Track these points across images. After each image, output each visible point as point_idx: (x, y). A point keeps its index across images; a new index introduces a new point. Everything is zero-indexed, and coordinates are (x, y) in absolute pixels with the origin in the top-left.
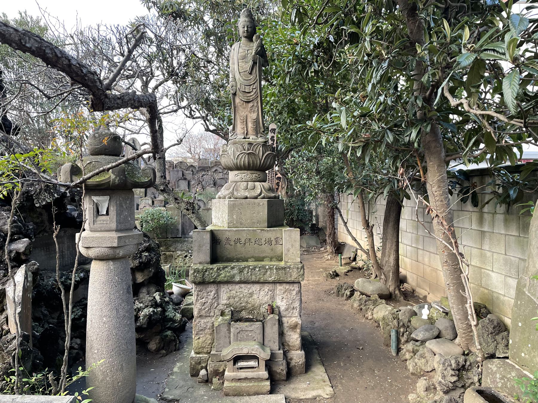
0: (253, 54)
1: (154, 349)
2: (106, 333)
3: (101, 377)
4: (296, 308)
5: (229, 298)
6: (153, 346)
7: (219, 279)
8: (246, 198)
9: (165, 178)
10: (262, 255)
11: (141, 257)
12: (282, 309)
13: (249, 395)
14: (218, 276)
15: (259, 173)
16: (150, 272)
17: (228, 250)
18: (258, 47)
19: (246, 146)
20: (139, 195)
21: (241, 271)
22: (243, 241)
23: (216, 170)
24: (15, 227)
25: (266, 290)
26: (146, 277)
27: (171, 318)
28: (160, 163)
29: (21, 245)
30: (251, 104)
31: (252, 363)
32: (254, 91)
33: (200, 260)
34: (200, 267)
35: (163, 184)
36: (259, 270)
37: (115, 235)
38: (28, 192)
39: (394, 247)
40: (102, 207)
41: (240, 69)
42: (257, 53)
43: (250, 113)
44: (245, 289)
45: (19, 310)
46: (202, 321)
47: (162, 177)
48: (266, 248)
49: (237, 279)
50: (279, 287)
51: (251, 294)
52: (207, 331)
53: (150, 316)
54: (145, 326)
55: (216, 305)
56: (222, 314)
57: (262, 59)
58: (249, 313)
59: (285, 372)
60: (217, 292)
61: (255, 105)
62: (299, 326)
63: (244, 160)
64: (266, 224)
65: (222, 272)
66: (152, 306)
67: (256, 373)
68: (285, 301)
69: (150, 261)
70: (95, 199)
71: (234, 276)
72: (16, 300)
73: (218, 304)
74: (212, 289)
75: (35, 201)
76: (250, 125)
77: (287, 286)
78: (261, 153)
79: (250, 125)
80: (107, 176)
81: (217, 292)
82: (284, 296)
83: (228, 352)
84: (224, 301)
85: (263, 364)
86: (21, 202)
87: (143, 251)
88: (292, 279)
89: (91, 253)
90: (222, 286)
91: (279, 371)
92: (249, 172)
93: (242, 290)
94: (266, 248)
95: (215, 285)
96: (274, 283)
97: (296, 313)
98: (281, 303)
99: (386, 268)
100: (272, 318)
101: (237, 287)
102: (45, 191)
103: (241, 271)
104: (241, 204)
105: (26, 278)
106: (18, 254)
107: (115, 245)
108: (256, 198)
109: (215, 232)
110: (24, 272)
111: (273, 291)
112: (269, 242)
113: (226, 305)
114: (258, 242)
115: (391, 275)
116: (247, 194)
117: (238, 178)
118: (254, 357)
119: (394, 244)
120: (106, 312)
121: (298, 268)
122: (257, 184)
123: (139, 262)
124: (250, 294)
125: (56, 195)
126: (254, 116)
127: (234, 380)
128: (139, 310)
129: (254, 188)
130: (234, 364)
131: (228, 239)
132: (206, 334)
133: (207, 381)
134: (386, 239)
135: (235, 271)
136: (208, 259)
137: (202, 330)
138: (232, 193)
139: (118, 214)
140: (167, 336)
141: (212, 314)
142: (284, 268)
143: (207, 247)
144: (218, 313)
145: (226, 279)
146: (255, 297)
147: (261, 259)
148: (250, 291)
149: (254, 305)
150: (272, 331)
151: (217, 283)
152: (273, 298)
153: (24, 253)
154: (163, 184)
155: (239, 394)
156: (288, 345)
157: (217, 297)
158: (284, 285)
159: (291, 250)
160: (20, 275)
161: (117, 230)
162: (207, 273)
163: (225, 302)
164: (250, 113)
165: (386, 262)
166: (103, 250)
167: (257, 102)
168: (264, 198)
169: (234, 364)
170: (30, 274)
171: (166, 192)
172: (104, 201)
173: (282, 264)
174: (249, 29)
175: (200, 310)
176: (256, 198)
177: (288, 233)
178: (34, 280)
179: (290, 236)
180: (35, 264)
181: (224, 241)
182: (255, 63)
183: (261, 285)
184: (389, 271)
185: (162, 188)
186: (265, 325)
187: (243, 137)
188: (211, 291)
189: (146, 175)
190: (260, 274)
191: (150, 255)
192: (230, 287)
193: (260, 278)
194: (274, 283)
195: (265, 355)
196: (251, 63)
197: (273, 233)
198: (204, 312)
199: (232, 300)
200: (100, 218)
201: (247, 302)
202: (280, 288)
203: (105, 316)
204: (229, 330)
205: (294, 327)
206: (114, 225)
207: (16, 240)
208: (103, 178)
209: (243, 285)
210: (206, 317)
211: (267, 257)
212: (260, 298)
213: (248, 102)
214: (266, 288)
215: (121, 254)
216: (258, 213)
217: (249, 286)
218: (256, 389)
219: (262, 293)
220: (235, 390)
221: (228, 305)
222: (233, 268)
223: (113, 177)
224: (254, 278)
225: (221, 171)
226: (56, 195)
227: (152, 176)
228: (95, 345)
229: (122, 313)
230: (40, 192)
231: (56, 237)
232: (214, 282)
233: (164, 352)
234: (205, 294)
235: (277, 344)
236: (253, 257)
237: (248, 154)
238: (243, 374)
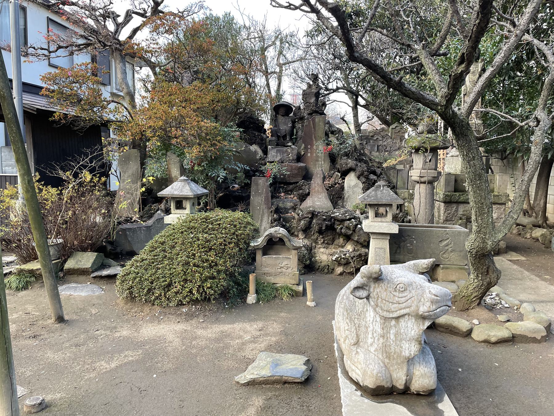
0: (479, 70)
4: (503, 218)
5: (464, 211)
7: (460, 200)
23: (377, 138)
33: (448, 190)
34: (449, 194)
39: (544, 194)
60: (457, 208)
65: (461, 197)
74: (454, 207)
81: (457, 208)
82: (496, 211)
88: (502, 202)
90: (460, 204)
99: (536, 209)
113: (462, 214)
115: (541, 214)
119: (545, 192)
134: (539, 189)
136: (453, 190)
141: (453, 219)
145: (463, 201)
157: (457, 211)
163: (461, 213)
165: (538, 204)
177: (501, 176)
179: (502, 178)
184: (540, 211)
188: (454, 207)
198: (449, 218)
199: (465, 213)
225: (381, 139)
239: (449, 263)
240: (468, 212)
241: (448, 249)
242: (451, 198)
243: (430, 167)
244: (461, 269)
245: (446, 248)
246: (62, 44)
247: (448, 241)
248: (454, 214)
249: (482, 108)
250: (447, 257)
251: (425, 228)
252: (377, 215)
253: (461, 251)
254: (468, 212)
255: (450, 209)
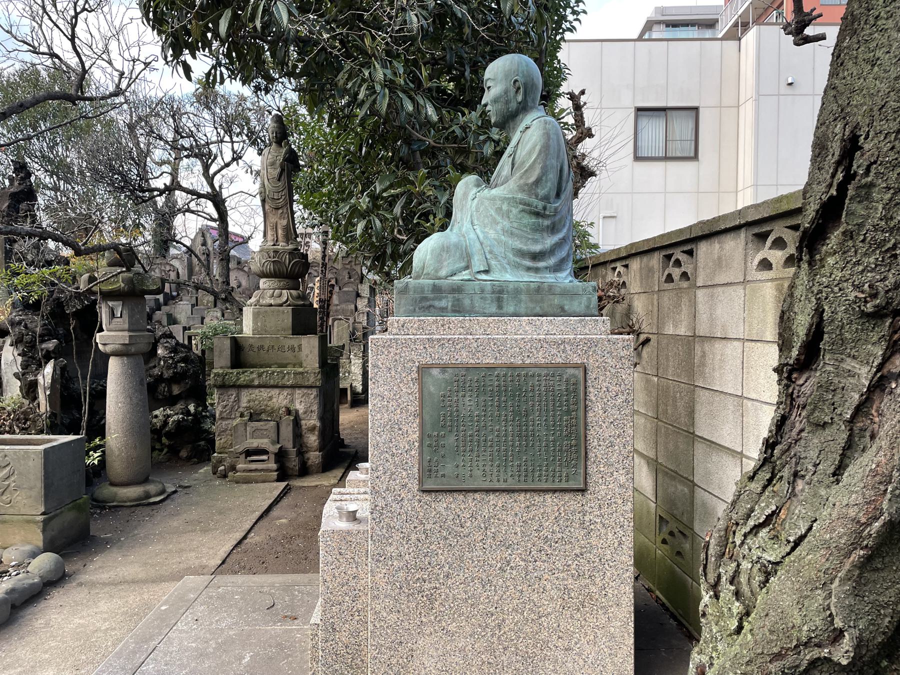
1: (185, 456)
2: (121, 417)
3: (117, 453)
4: (314, 411)
5: (249, 401)
6: (184, 454)
7: (238, 383)
8: (271, 305)
9: (228, 284)
10: (285, 362)
11: (176, 368)
12: (301, 412)
13: (257, 482)
14: (238, 379)
15: (287, 280)
16: (187, 383)
17: (250, 356)
18: (286, 154)
19: (272, 254)
20: (207, 305)
21: (260, 375)
22: (266, 348)
24: (45, 329)
25: (285, 394)
26: (183, 389)
27: (206, 430)
28: (222, 265)
29: (51, 345)
30: (280, 211)
31: (265, 457)
32: (283, 197)
33: (220, 365)
34: (221, 371)
35: (224, 292)
36: (277, 375)
37: (126, 334)
38: (58, 299)
40: (117, 311)
41: (269, 175)
42: (285, 160)
43: (280, 219)
44: (265, 393)
45: (48, 393)
46: (224, 423)
47: (224, 282)
48: (289, 354)
49: (256, 383)
50: (298, 391)
51: (271, 398)
52: (228, 432)
53: (178, 421)
54: (173, 431)
55: (236, 407)
56: (242, 415)
57: (290, 166)
58: (268, 416)
59: (297, 468)
61: (285, 211)
62: (317, 429)
63: (270, 267)
64: (290, 332)
66: (182, 413)
67: (265, 466)
68: (303, 404)
69: (187, 372)
70: (110, 303)
71: (253, 380)
72: (46, 385)
73: (239, 407)
74: (233, 393)
75: (66, 308)
76: (280, 232)
77: (305, 391)
78: (287, 261)
79: (280, 232)
80: (118, 285)
81: (238, 396)
82: (302, 399)
83: (240, 448)
84: (244, 403)
85: (272, 457)
86: (52, 308)
87: (179, 362)
88: (310, 383)
89: (108, 349)
91: (291, 466)
92: (277, 279)
93: (262, 394)
94: (289, 354)
95: (236, 389)
96: (293, 387)
97: (315, 416)
98: (300, 407)
100: (287, 421)
101: (257, 391)
102: (76, 297)
103: (260, 375)
104: (266, 312)
105: (54, 370)
106: (48, 352)
107: (127, 342)
108: (281, 305)
109: (238, 339)
110: (53, 365)
111: (292, 395)
112: (292, 349)
113: (246, 407)
114: (281, 348)
116: (272, 302)
117: (266, 286)
118: (264, 452)
120: (121, 399)
121: (315, 373)
122: (284, 292)
123: (174, 372)
124: (270, 397)
125: (86, 302)
126: (285, 222)
127: (244, 471)
128: (169, 416)
129: (280, 295)
130: (246, 458)
131: (251, 346)
132: (227, 435)
133: (225, 476)
135: (254, 375)
136: (229, 364)
137: (223, 431)
138: (258, 301)
139: (130, 317)
140: (200, 445)
141: (233, 416)
142: (302, 373)
143: (227, 353)
144: (238, 415)
145: (245, 383)
146: (274, 400)
147: (285, 366)
148: (270, 395)
149: (273, 408)
150: (287, 431)
151: (240, 387)
152: (292, 401)
153: (53, 351)
154: (224, 292)
155: (247, 481)
156: (307, 447)
157: (238, 400)
158: (303, 390)
159: (310, 356)
160: (49, 369)
161: (129, 330)
162: (227, 377)
163: (245, 405)
164: (280, 219)
166: (117, 346)
167: (287, 209)
168: (289, 305)
169: (246, 458)
170: (58, 368)
171: (229, 302)
172: (119, 306)
173: (301, 370)
174: (278, 135)
175: (221, 412)
176: (281, 305)
178: (62, 375)
180: (63, 361)
181: (247, 349)
182: (282, 170)
183: (280, 389)
185: (223, 296)
186: (280, 425)
187: (272, 244)
188: (232, 395)
189: (154, 283)
190: (278, 379)
191: (186, 367)
192: (251, 391)
193: (278, 382)
194: (293, 387)
195: (274, 449)
196: (279, 170)
197: (294, 341)
198: (225, 414)
199: (252, 404)
200: (115, 320)
201: (266, 405)
202: (298, 392)
203: (120, 402)
204: (246, 429)
205: (312, 429)
206: (126, 326)
207: (47, 340)
208: (764, 230)
209: (262, 390)
210: (228, 419)
211: (290, 364)
212: (279, 401)
213: (278, 209)
214: (285, 392)
215: (133, 350)
216: (283, 321)
217: (268, 390)
218: (264, 478)
219: (281, 397)
220: (244, 479)
221: (248, 408)
222: (252, 373)
223: (123, 285)
224: (272, 382)
226: (86, 302)
227: (160, 284)
228: (113, 427)
229: (135, 401)
230: (70, 299)
231: (73, 329)
232: (234, 386)
233: (196, 460)
234: (226, 397)
235: (291, 442)
236: (276, 364)
237: (273, 262)
238: (254, 466)
239: (11, 511)
240: (257, 402)
241: (9, 485)
242: (224, 379)
243: (121, 327)
244: (28, 522)
245: (6, 483)
246: (94, 47)
247: (8, 469)
248: (233, 407)
249: (26, 223)
250: (9, 499)
251: (13, 447)
252: (360, 400)
253: (31, 489)
254: (257, 402)
255: (226, 397)
